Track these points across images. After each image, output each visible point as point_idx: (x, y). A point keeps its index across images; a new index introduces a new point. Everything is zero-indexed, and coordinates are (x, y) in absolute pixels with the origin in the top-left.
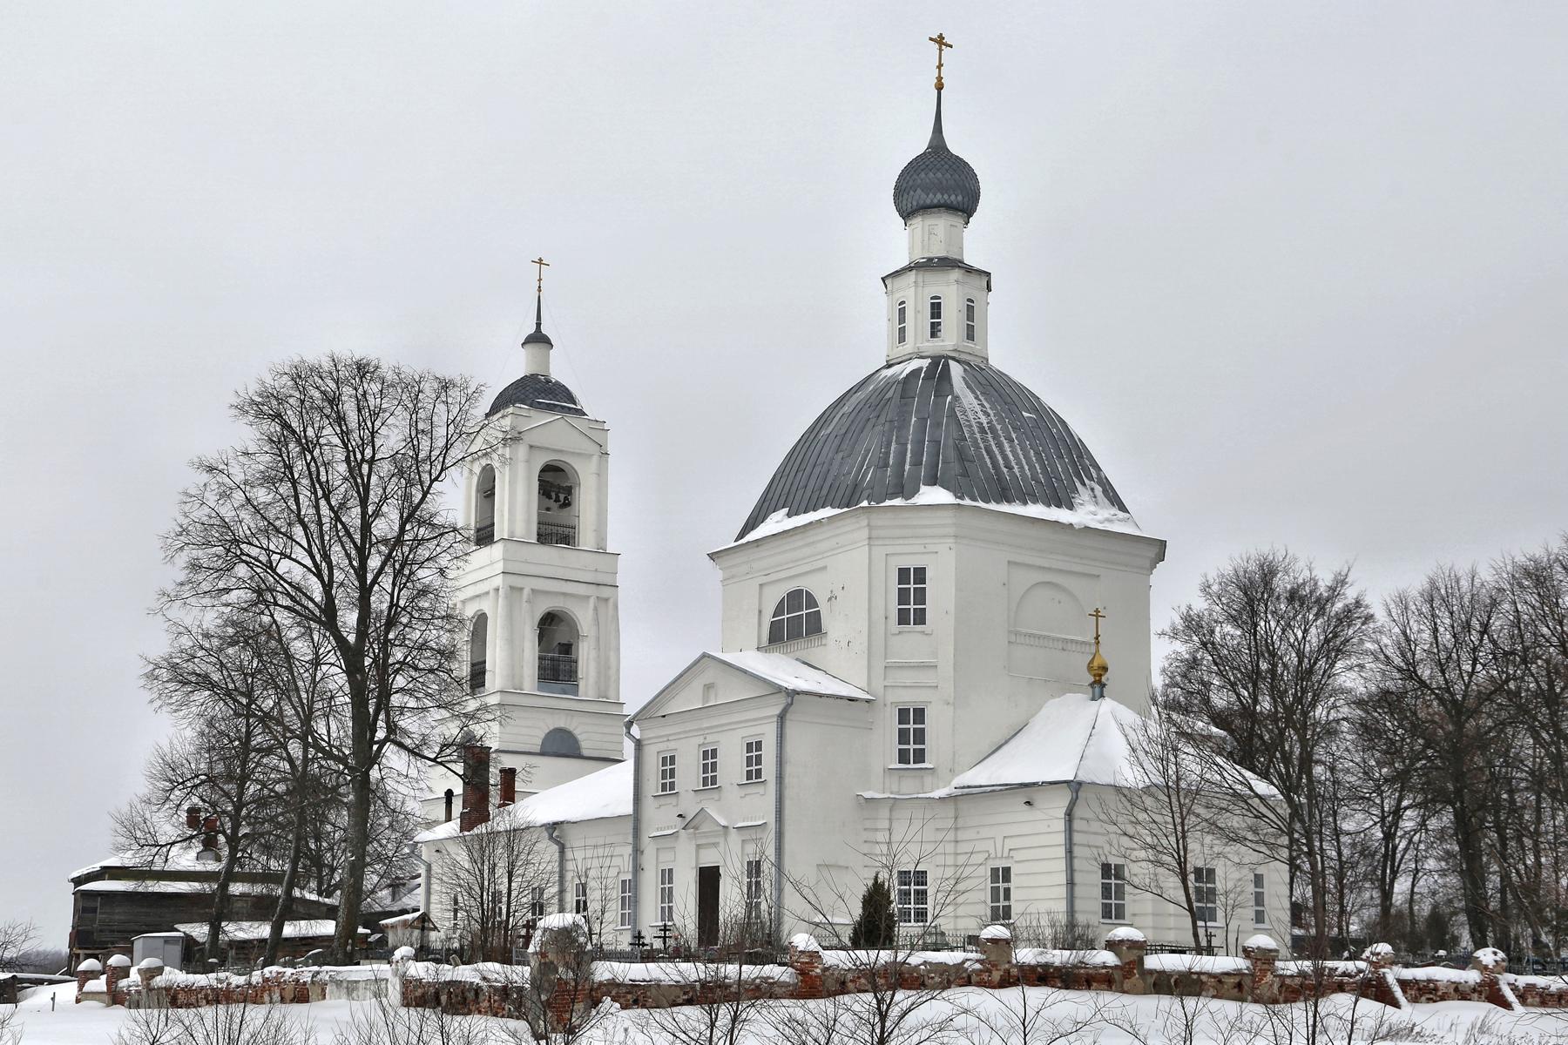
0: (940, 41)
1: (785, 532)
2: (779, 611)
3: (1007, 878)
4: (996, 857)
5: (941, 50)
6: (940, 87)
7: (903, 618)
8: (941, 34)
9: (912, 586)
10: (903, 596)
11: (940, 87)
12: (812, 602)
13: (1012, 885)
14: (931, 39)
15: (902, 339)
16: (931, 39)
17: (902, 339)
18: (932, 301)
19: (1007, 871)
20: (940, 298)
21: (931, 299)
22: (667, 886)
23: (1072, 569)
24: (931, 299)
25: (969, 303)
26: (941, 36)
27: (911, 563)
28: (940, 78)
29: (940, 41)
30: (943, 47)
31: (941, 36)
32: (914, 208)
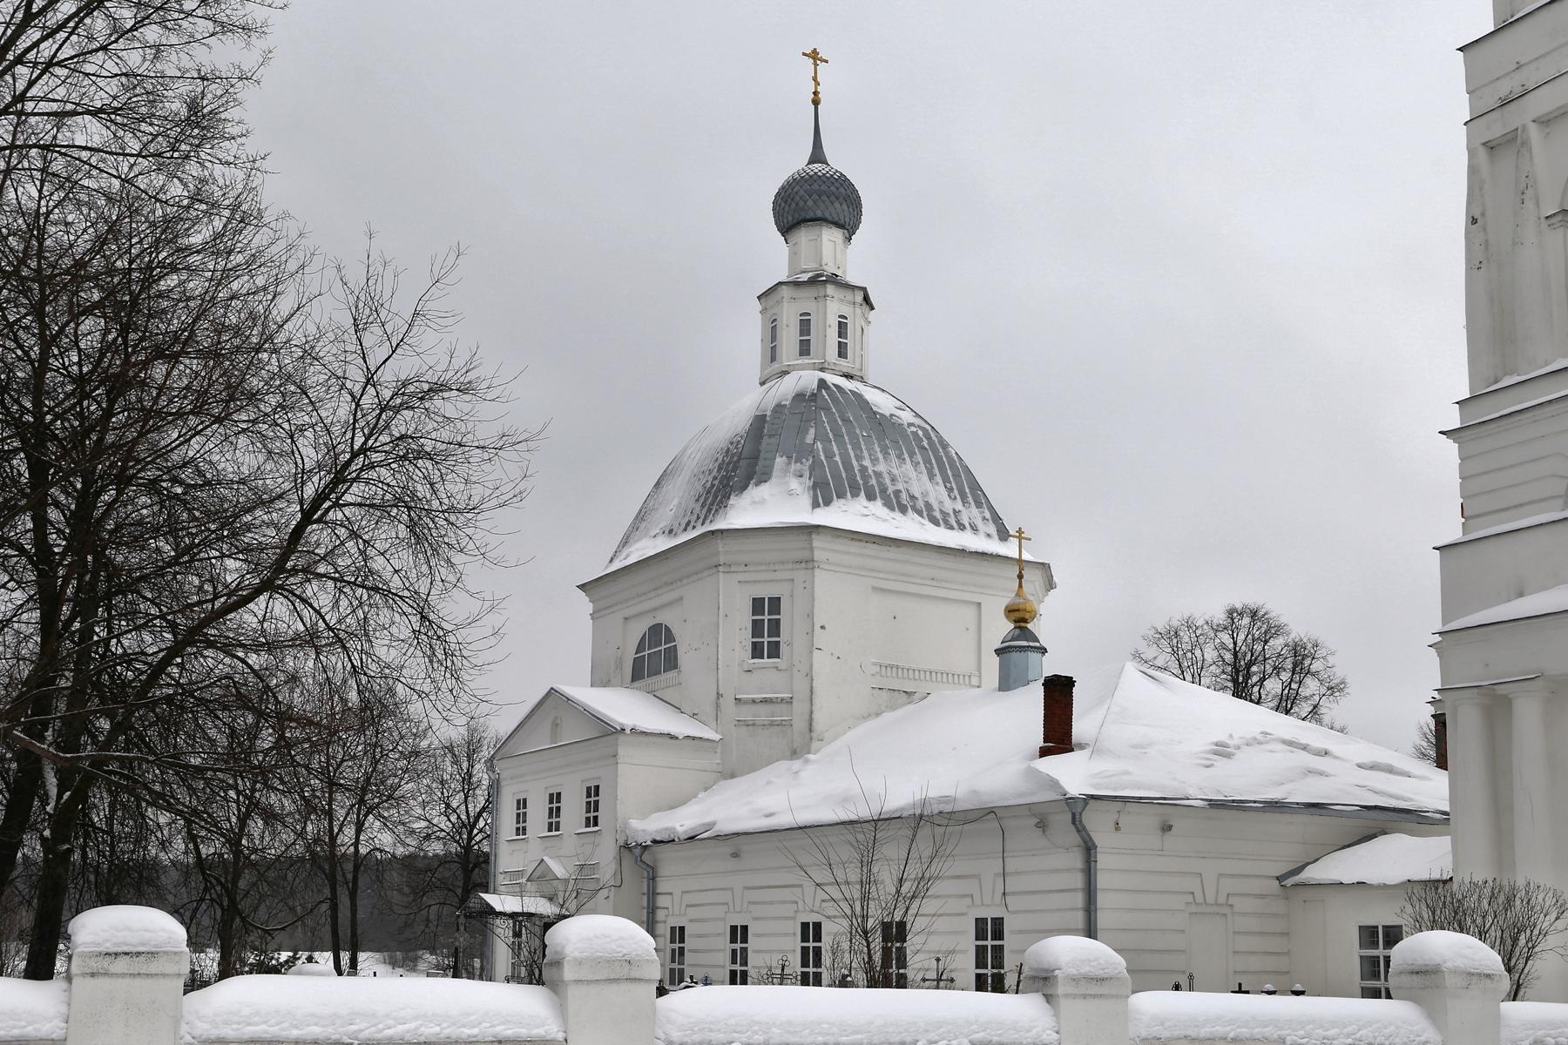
0: (814, 56)
1: (983, 554)
2: (640, 648)
3: (998, 934)
4: (680, 915)
5: (816, 65)
6: (816, 102)
7: (757, 651)
8: (815, 49)
9: (766, 617)
10: (775, 627)
11: (816, 102)
12: (670, 637)
13: (799, 944)
14: (804, 54)
15: (773, 359)
16: (804, 54)
17: (773, 359)
18: (840, 320)
19: (998, 923)
20: (809, 314)
21: (801, 315)
22: (811, 944)
23: (933, 594)
24: (801, 315)
25: (840, 320)
26: (815, 51)
27: (766, 592)
28: (816, 93)
29: (814, 56)
30: (818, 62)
31: (815, 51)
32: (790, 224)
